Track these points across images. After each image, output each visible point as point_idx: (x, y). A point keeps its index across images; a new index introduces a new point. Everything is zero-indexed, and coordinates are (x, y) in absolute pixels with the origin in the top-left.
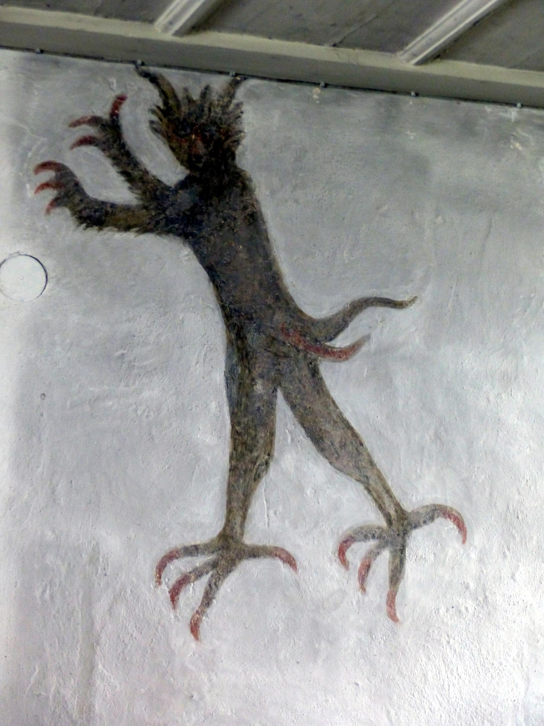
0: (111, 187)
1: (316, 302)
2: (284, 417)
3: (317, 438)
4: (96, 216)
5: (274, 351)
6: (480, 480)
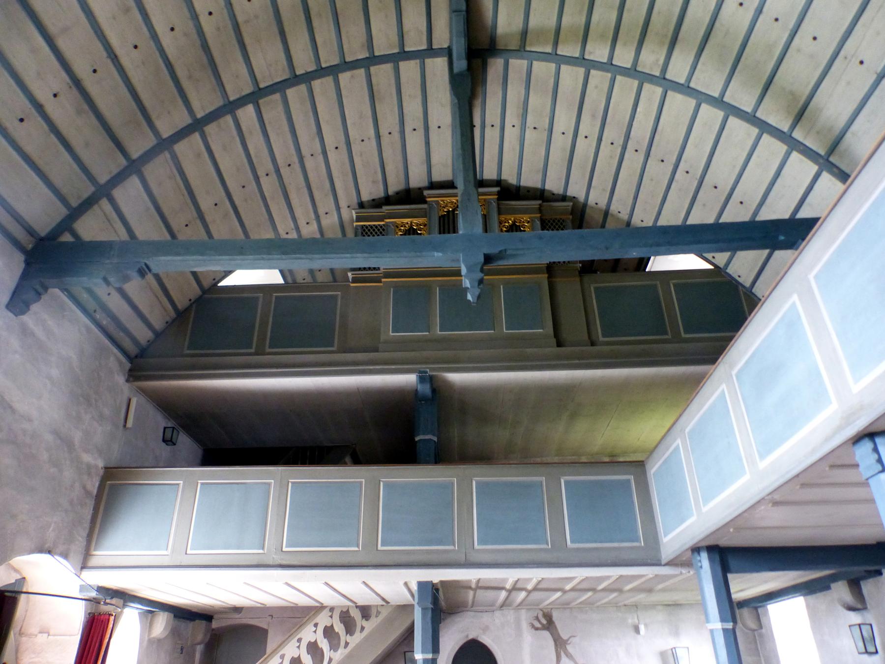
0: (538, 625)
1: (564, 636)
2: (562, 653)
3: (567, 656)
4: (537, 629)
5: (560, 644)
6: (52, 470)
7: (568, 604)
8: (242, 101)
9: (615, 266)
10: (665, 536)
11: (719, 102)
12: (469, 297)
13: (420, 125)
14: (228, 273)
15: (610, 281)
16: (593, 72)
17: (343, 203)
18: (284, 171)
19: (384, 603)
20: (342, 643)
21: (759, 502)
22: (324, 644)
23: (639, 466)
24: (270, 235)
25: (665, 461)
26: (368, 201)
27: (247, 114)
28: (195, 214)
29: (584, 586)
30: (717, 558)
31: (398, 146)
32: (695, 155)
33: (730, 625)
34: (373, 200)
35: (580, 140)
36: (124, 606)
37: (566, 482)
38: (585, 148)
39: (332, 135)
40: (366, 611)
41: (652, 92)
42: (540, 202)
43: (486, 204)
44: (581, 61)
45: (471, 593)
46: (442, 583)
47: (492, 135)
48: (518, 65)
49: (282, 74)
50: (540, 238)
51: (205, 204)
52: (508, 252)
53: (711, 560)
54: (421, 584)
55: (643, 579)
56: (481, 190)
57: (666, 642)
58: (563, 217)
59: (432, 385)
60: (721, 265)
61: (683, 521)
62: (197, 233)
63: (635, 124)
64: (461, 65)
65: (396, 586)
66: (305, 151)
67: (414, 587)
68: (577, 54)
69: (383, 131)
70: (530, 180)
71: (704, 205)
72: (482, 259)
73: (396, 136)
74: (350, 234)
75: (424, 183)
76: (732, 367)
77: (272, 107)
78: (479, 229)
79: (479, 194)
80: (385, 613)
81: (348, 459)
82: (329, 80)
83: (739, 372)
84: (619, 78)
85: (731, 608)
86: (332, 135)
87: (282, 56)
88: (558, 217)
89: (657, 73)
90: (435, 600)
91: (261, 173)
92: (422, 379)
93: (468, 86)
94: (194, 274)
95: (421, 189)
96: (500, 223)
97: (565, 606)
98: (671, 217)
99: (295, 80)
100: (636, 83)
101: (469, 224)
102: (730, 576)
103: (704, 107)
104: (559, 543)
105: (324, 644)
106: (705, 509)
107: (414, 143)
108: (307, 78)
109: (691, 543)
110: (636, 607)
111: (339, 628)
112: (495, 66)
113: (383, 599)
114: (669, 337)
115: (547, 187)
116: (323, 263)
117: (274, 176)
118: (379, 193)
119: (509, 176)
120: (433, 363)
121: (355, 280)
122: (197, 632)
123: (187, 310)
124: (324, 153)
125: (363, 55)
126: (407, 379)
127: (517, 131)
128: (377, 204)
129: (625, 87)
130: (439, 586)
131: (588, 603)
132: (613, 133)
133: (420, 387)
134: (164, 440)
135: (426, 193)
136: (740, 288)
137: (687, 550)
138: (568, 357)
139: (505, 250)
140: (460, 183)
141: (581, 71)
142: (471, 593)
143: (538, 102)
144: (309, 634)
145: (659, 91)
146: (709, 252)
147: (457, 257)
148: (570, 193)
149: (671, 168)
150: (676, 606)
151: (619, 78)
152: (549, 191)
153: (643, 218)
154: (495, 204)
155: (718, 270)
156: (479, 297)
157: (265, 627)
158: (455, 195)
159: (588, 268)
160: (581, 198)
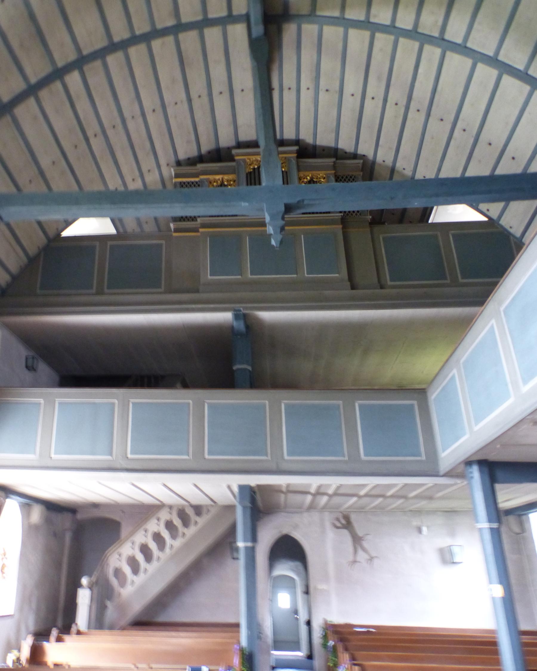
0: (339, 525)
4: (338, 528)
7: (363, 508)
8: (68, 68)
9: (401, 217)
10: (444, 451)
11: (492, 61)
12: (273, 242)
13: (225, 88)
14: (68, 223)
15: (399, 232)
16: (378, 35)
17: (163, 162)
18: (110, 133)
19: (212, 503)
20: (180, 534)
21: (521, 421)
22: (166, 534)
23: (420, 393)
24: (102, 188)
25: (443, 389)
26: (184, 160)
27: (74, 79)
28: (36, 171)
29: (373, 492)
30: (486, 470)
31: (208, 107)
32: (471, 114)
33: (495, 525)
34: (189, 159)
35: (368, 102)
36: (7, 497)
37: (360, 406)
38: (372, 108)
39: (149, 101)
40: (198, 510)
41: (432, 53)
42: (333, 160)
43: (286, 161)
44: (366, 24)
45: (282, 496)
46: (259, 486)
47: (289, 98)
48: (309, 29)
49: (101, 43)
50: (333, 189)
51: (45, 162)
52: (306, 202)
53: (481, 471)
54: (242, 488)
55: (424, 488)
56: (281, 149)
57: (444, 541)
58: (354, 174)
59: (245, 322)
60: (495, 216)
61: (457, 438)
62: (39, 187)
63: (417, 84)
64: (258, 30)
65: (221, 488)
66: (127, 114)
67: (236, 489)
68: (362, 18)
69: (194, 95)
70: (325, 139)
71: (480, 161)
72: (283, 209)
73: (205, 99)
74: (169, 186)
75: (233, 143)
76: (500, 304)
77: (94, 71)
78: (279, 181)
79: (280, 153)
80: (213, 511)
81: (179, 385)
82: (142, 47)
83: (507, 308)
84: (402, 40)
85: (497, 514)
86: (149, 101)
87: (100, 23)
88: (351, 174)
89: (436, 34)
90: (253, 500)
91: (90, 134)
92: (237, 317)
93: (266, 51)
94: (39, 223)
95: (229, 149)
96: (300, 179)
97: (360, 510)
98: (451, 170)
99: (113, 47)
100: (417, 45)
101: (271, 178)
102: (498, 486)
103: (480, 66)
104: (354, 456)
105: (166, 534)
106: (476, 428)
107: (222, 105)
108: (123, 46)
109: (463, 458)
110: (419, 512)
111: (177, 522)
112: (289, 31)
113: (212, 500)
114: (448, 281)
115: (340, 146)
116: (147, 213)
117: (101, 137)
118: (193, 152)
119: (306, 136)
120: (246, 303)
121: (176, 231)
122: (65, 522)
123: (38, 256)
124: (143, 115)
125: (171, 22)
126: (224, 317)
127: (311, 93)
128: (191, 162)
129: (407, 48)
130: (256, 490)
131: (380, 509)
132: (397, 95)
133: (235, 324)
134: (27, 367)
135: (234, 152)
136: (512, 238)
137: (460, 463)
138: (362, 299)
139: (303, 201)
140: (262, 143)
141: (367, 34)
142: (282, 496)
143: (329, 65)
144: (155, 526)
145: (438, 51)
146: (483, 201)
147: (260, 208)
148: (360, 151)
149: (449, 126)
150: (451, 512)
151: (402, 40)
152: (342, 150)
153: (426, 172)
154: (294, 162)
155: (491, 223)
156: (281, 242)
157: (117, 519)
158: (258, 154)
159: (379, 218)
160: (370, 155)
